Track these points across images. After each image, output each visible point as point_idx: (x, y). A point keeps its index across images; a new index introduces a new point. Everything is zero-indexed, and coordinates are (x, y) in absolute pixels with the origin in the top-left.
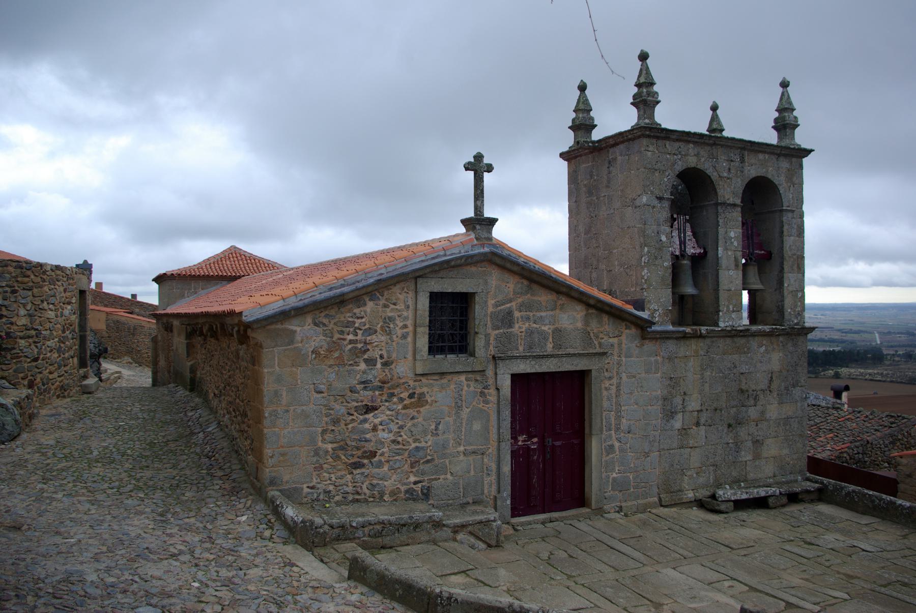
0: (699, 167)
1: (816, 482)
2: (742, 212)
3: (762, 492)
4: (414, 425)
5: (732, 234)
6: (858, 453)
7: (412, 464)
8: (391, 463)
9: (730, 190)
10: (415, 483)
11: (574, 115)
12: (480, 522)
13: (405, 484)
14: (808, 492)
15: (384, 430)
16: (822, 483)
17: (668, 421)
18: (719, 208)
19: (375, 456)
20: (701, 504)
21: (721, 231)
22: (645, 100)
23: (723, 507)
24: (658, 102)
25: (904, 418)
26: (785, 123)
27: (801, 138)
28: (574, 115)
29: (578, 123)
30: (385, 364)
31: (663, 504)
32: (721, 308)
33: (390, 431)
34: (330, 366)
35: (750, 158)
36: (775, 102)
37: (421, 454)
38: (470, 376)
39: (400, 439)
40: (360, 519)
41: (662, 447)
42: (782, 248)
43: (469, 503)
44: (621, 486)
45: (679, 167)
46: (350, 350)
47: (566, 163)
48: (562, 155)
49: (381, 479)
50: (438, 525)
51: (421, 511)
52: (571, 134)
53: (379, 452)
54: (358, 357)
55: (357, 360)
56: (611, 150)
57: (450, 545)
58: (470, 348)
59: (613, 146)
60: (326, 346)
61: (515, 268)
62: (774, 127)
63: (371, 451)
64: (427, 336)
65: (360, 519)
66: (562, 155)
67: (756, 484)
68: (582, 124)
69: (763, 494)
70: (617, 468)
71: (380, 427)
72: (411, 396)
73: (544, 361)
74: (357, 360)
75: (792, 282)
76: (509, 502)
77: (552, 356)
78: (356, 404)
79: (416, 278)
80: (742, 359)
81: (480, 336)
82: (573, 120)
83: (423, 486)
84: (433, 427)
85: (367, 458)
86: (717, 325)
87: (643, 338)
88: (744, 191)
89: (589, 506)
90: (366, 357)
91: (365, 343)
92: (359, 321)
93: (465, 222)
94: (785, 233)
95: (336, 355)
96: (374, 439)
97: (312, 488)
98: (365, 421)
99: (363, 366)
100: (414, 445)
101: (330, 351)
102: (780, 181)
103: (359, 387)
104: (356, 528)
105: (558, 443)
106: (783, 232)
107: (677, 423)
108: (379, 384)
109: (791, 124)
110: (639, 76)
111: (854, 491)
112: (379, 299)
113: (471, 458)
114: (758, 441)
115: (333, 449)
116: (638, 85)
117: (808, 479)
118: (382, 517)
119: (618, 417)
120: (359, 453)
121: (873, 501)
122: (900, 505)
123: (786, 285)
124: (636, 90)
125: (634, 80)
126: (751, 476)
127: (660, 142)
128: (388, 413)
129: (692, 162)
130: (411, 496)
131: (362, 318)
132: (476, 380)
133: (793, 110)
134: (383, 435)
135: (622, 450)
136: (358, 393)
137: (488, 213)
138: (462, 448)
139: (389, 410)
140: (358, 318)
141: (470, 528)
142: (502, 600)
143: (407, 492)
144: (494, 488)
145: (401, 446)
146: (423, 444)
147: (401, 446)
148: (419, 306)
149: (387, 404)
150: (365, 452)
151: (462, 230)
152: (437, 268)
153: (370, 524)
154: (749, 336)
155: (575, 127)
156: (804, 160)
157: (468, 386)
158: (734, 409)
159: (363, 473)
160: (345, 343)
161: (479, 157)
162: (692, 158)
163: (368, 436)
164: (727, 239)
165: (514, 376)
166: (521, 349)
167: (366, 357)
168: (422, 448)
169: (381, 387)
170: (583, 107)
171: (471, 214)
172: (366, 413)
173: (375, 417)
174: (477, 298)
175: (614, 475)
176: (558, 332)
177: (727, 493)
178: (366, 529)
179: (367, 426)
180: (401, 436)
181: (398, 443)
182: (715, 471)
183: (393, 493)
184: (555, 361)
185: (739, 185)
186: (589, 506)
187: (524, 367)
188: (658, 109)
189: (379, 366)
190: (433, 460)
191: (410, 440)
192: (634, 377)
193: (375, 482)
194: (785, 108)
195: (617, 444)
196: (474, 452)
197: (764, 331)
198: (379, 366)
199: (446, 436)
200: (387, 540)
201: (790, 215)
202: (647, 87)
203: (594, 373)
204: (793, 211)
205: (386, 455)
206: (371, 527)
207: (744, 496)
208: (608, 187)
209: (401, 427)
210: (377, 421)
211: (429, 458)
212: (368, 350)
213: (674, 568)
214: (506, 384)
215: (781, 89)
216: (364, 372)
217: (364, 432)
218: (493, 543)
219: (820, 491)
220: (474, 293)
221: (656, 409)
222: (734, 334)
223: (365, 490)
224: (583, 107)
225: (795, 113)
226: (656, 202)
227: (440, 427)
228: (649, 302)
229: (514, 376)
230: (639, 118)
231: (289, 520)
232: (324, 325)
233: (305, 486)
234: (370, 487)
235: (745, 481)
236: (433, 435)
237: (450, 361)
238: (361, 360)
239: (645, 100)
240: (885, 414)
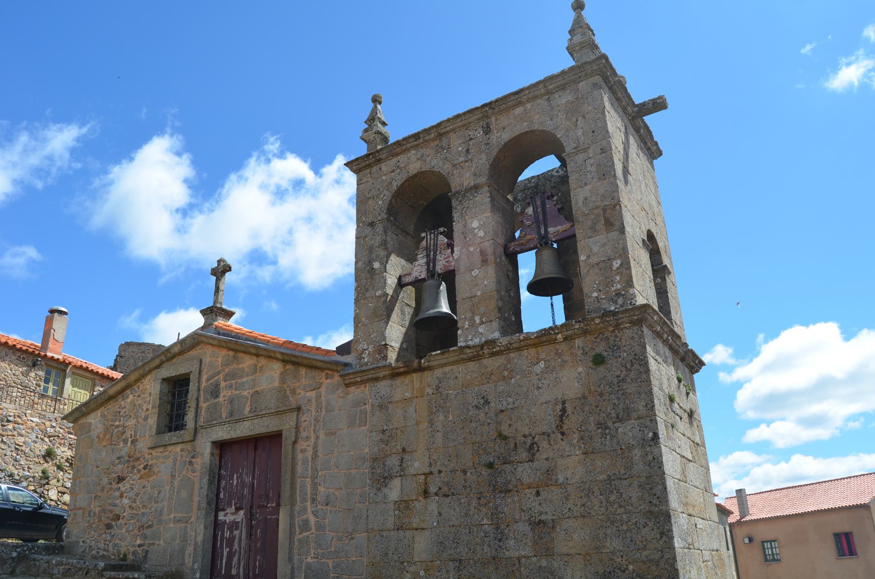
10: (140, 546)
17: (379, 489)
103: (117, 462)
113: (178, 525)
175: (309, 560)
187: (222, 433)
195: (312, 520)
211: (150, 523)
215: (372, 105)
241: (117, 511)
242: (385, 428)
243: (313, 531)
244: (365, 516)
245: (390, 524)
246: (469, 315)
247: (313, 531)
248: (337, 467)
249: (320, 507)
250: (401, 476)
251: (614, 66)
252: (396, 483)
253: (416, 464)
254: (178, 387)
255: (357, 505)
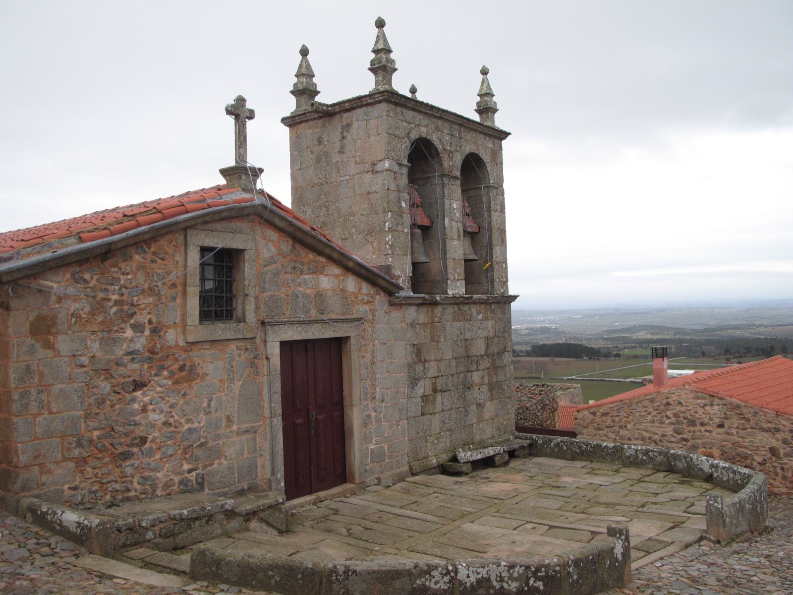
0: (428, 138)
1: (526, 439)
2: (462, 185)
3: (490, 452)
4: (186, 403)
5: (455, 206)
6: (521, 419)
7: (185, 449)
8: (163, 450)
9: (453, 163)
10: (190, 471)
11: (295, 80)
12: (271, 507)
13: (180, 474)
14: (523, 447)
15: (154, 410)
16: (531, 439)
17: (413, 388)
18: (445, 179)
19: (145, 443)
20: (444, 470)
21: (447, 202)
22: (382, 66)
23: (464, 469)
24: (395, 70)
25: (548, 386)
26: (486, 109)
27: (500, 121)
28: (295, 80)
29: (301, 87)
30: (154, 331)
31: (414, 472)
32: (449, 276)
33: (162, 412)
34: (94, 333)
35: (468, 136)
36: (476, 87)
37: (194, 436)
38: (241, 344)
39: (171, 420)
40: (150, 517)
41: (409, 415)
42: (490, 222)
43: (244, 490)
44: (378, 457)
45: (414, 136)
46: (115, 313)
47: (288, 129)
48: (284, 120)
49: (153, 470)
50: (231, 514)
51: (206, 500)
52: (293, 100)
53: (151, 437)
54: (124, 322)
55: (123, 325)
56: (345, 115)
57: (246, 535)
58: (238, 312)
59: (348, 110)
60: (88, 308)
61: (282, 225)
62: (476, 110)
63: (141, 437)
64: (198, 298)
65: (150, 517)
66: (284, 120)
67: (482, 445)
68: (305, 90)
69: (492, 453)
70: (374, 439)
71: (151, 407)
72: (182, 368)
73: (309, 327)
74: (123, 325)
75: (499, 253)
76: (282, 484)
77: (316, 322)
78: (123, 380)
79: (185, 229)
80: (466, 326)
81: (250, 298)
82: (295, 85)
83: (197, 475)
84: (205, 404)
85: (137, 445)
86: (446, 293)
87: (391, 304)
88: (462, 165)
89: (352, 481)
90: (132, 321)
91: (132, 305)
92: (125, 277)
93: (225, 172)
94: (492, 208)
95: (100, 318)
96: (143, 422)
97: (75, 489)
98: (134, 400)
99: (129, 333)
100: (186, 427)
101: (92, 314)
102: (486, 158)
103: (126, 359)
104: (146, 529)
105: (320, 417)
106: (490, 207)
107: (420, 390)
108: (148, 354)
109: (493, 108)
110: (377, 42)
111: (562, 442)
112: (145, 252)
113: (244, 438)
114: (480, 404)
115: (99, 438)
116: (376, 51)
117: (517, 437)
118: (173, 512)
119: (374, 386)
120: (128, 440)
121: (580, 447)
122: (606, 446)
123: (494, 257)
124: (373, 56)
125: (371, 46)
126: (477, 438)
127: (398, 109)
128: (158, 389)
129: (423, 131)
130: (186, 488)
131: (128, 274)
132: (247, 349)
133: (493, 95)
134: (153, 416)
135: (378, 421)
136: (125, 366)
137: (252, 160)
138: (235, 427)
139: (160, 386)
140: (123, 274)
141: (262, 515)
142: (403, 561)
143: (181, 483)
144: (268, 469)
145: (172, 429)
146: (196, 425)
147: (172, 429)
148: (190, 263)
149: (156, 379)
150: (135, 438)
151: (222, 181)
152: (208, 219)
153: (161, 522)
154: (471, 303)
155: (298, 92)
156: (504, 142)
157: (239, 355)
158: (462, 375)
159: (133, 465)
160: (111, 304)
161: (241, 101)
162: (424, 129)
163: (137, 418)
164: (451, 209)
165: (284, 344)
166: (287, 314)
167: (132, 321)
168: (195, 430)
169: (150, 359)
170: (305, 72)
171: (232, 163)
172: (134, 390)
173: (144, 394)
174: (247, 256)
175: (372, 447)
176: (319, 295)
177: (465, 456)
178: (156, 528)
179: (136, 406)
180: (173, 416)
181: (170, 425)
182: (450, 436)
183: (166, 486)
184: (319, 327)
185: (458, 159)
186: (352, 482)
187: (292, 334)
188: (395, 76)
189: (147, 333)
190: (206, 443)
191: (183, 421)
192: (385, 344)
193: (146, 474)
194: (486, 94)
195: (373, 414)
196: (247, 431)
197: (482, 299)
198: (147, 333)
199: (218, 414)
200: (179, 539)
201: (495, 191)
202: (385, 54)
203: (353, 341)
204: (497, 188)
205: (158, 441)
206: (162, 525)
207: (479, 457)
208: (340, 152)
209: (172, 407)
210: (146, 399)
211: (203, 440)
212: (135, 313)
213: (472, 522)
214: (275, 350)
215: (481, 77)
216: (131, 341)
217: (133, 413)
218: (284, 528)
219: (530, 445)
220: (243, 250)
221: (402, 377)
222: (458, 302)
223: (136, 485)
224: (305, 72)
225: (494, 99)
226: (396, 168)
227: (213, 403)
228: (394, 267)
229: (284, 344)
230: (377, 83)
231: (73, 528)
232: (86, 281)
233: (66, 487)
234: (141, 480)
235: (473, 443)
236: (208, 413)
237: (220, 330)
238: (128, 325)
239: (382, 66)
240: (531, 385)
241: (140, 431)
242: (415, 343)
243: (374, 423)
244: (405, 408)
245: (419, 413)
246: (453, 272)
247: (374, 423)
248: (388, 372)
249: (377, 404)
250: (424, 379)
251: (445, 108)
252: (421, 383)
253: (432, 371)
254: (224, 263)
255: (401, 400)
